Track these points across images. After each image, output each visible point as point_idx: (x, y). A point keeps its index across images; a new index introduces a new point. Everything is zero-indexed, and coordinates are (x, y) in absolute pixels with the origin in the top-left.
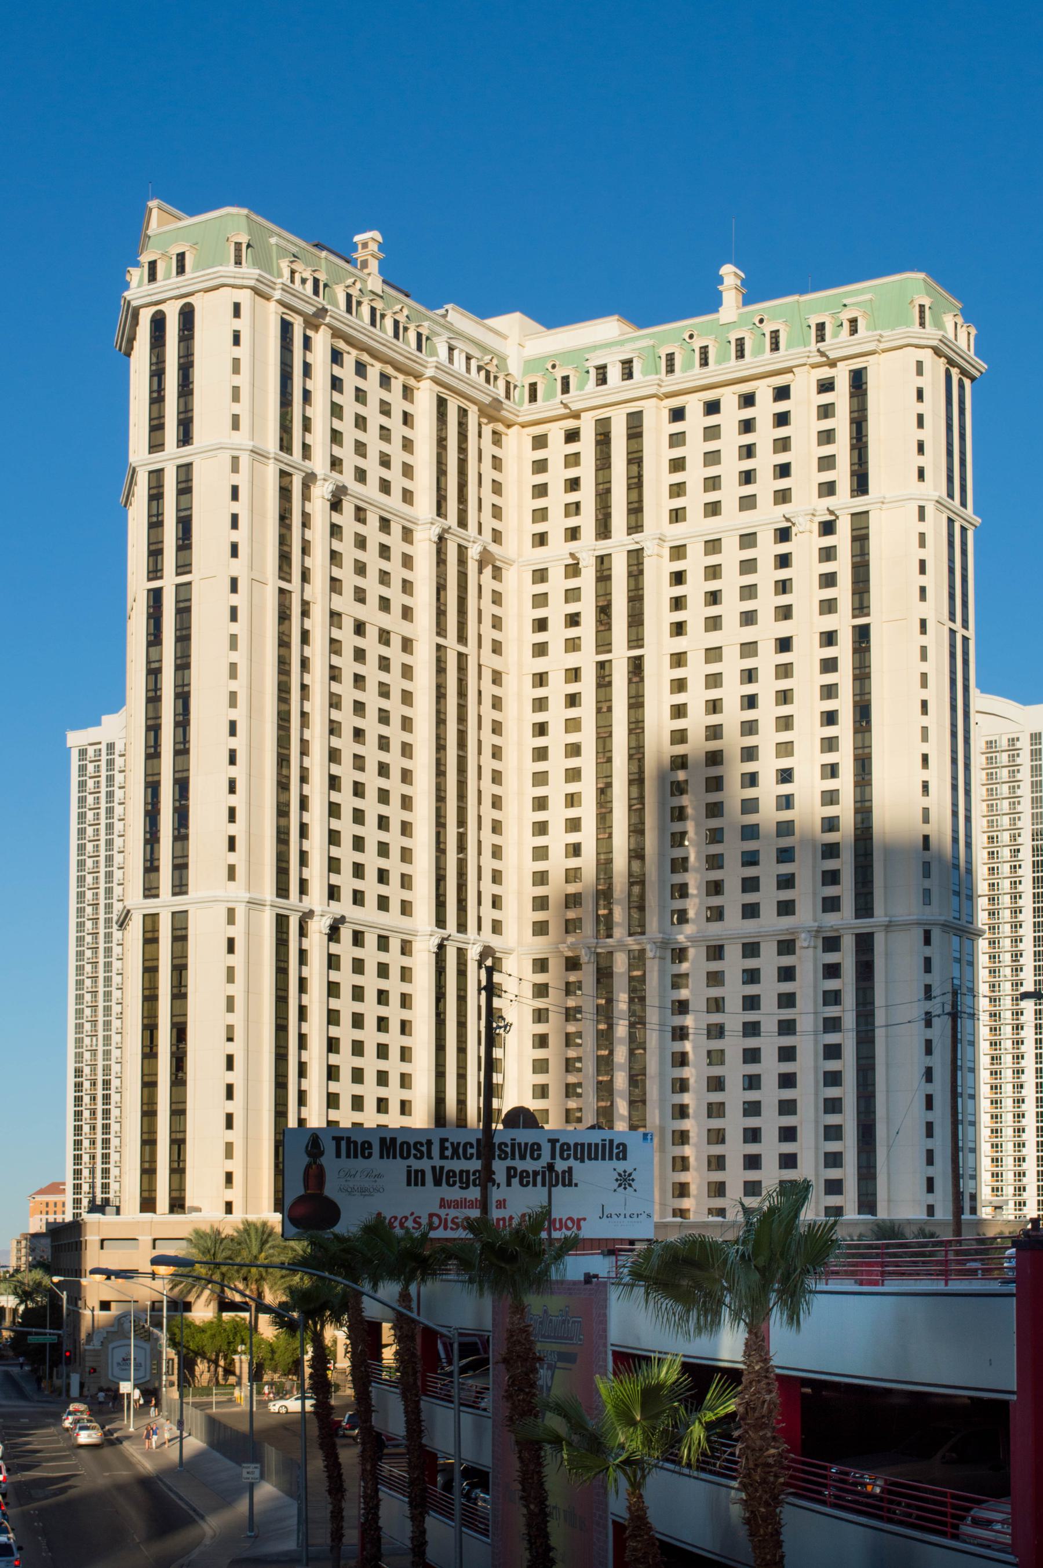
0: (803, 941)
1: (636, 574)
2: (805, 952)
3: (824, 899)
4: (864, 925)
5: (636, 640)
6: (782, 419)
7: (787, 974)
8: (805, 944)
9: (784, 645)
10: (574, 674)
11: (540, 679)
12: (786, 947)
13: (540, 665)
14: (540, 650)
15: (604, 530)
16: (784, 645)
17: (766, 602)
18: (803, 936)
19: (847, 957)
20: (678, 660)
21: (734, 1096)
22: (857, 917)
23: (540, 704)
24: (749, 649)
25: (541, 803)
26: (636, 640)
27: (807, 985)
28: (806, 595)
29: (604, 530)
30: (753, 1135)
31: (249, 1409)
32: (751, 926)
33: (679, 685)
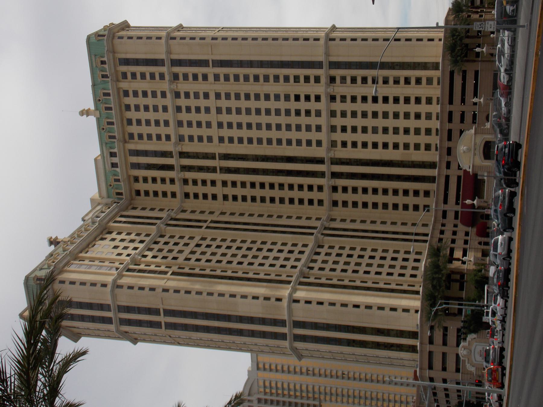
0: (330, 90)
1: (138, 153)
2: (335, 91)
3: (264, 82)
4: (325, 65)
5: (212, 157)
6: (187, 95)
7: (343, 98)
8: (175, 87)
9: (218, 96)
10: (224, 183)
11: (225, 197)
12: (177, 95)
13: (220, 197)
14: (214, 197)
15: (170, 168)
16: (218, 96)
17: (202, 103)
18: (172, 87)
19: (338, 73)
20: (221, 139)
21: (391, 123)
22: (322, 68)
23: (282, 201)
24: (219, 110)
25: (375, 205)
26: (212, 157)
27: (348, 90)
28: (201, 87)
29: (170, 168)
30: (375, 115)
31: (258, 357)
32: (324, 114)
33: (289, 142)
